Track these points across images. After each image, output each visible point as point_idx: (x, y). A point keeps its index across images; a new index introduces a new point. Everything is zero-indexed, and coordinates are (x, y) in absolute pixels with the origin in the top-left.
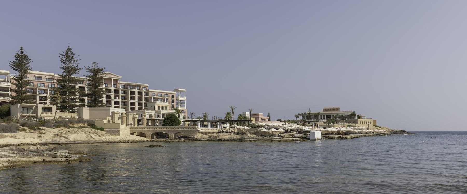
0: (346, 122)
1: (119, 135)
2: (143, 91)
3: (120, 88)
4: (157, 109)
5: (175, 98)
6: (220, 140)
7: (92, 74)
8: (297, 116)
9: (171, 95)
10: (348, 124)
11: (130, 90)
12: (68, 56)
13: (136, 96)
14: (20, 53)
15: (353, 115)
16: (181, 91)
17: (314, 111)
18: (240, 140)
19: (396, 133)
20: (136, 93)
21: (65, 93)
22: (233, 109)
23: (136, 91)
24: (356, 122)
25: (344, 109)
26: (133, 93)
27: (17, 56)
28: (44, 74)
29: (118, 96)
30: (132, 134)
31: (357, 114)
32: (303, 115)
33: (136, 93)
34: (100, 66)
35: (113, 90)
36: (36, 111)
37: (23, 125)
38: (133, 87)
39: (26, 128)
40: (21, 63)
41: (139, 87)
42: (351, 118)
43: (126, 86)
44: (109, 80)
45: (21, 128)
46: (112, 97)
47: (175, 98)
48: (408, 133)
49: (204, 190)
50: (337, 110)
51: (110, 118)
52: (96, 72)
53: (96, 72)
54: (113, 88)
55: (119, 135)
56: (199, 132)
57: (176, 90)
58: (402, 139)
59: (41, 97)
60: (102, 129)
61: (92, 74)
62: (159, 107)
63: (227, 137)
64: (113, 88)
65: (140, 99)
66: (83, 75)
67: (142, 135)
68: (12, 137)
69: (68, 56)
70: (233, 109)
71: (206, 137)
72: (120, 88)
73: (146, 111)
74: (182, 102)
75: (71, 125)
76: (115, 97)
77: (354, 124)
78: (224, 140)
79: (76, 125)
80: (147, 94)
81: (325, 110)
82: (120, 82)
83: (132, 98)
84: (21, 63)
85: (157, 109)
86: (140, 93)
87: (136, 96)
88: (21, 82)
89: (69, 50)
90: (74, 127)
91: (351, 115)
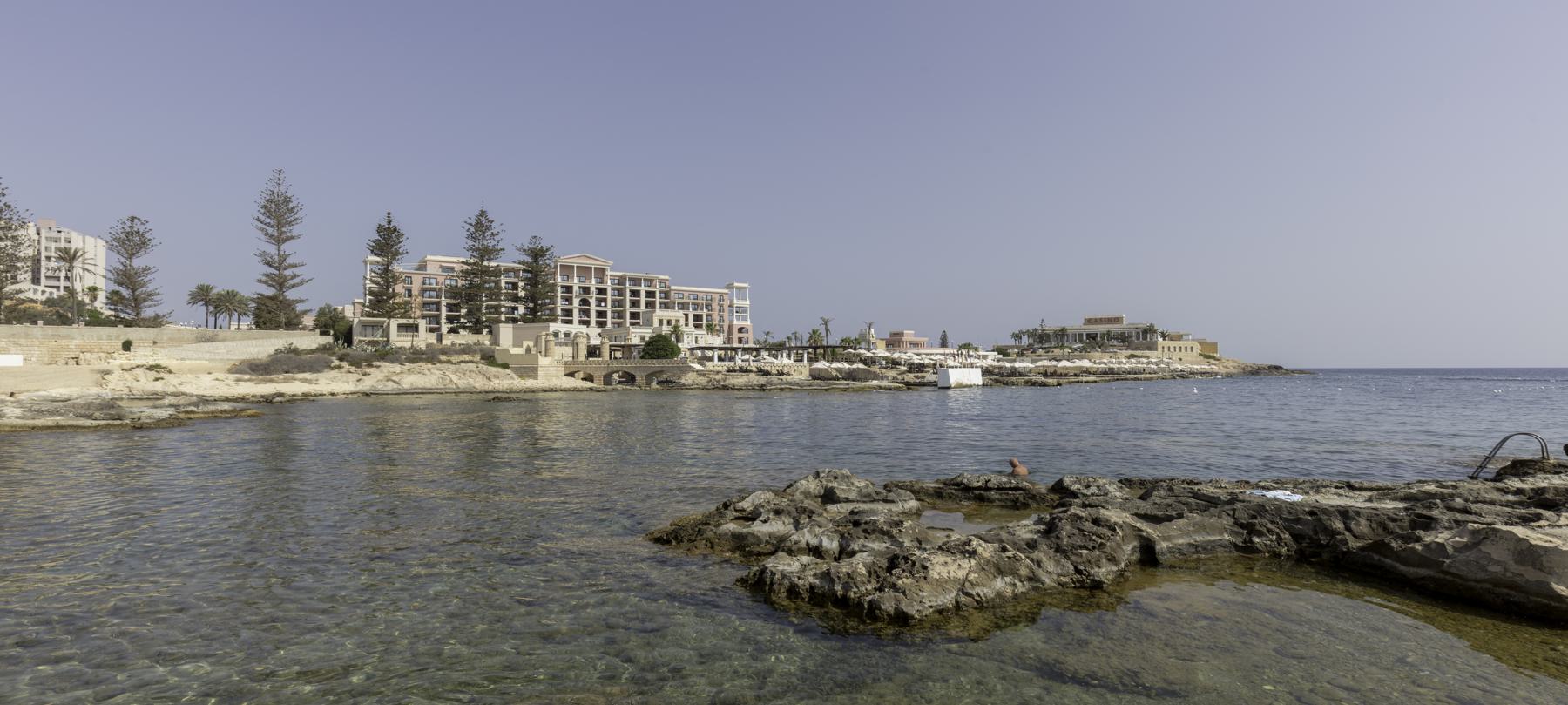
0: (1128, 348)
1: (536, 378)
2: (657, 289)
3: (608, 285)
4: (656, 324)
5: (727, 303)
6: (725, 387)
7: (529, 259)
8: (1017, 337)
9: (717, 297)
10: (1130, 352)
11: (629, 287)
12: (481, 226)
13: (643, 299)
14: (385, 223)
15: (1149, 331)
16: (739, 289)
17: (1052, 325)
18: (762, 388)
19: (1257, 371)
20: (643, 294)
21: (472, 301)
22: (826, 323)
23: (643, 290)
24: (1152, 347)
25: (1132, 319)
26: (635, 293)
27: (380, 229)
28: (436, 259)
29: (605, 300)
30: (571, 375)
31: (1159, 328)
32: (1031, 334)
33: (643, 294)
34: (545, 244)
35: (593, 289)
36: (386, 334)
37: (341, 359)
38: (636, 281)
39: (344, 364)
40: (387, 242)
41: (650, 281)
42: (1144, 338)
43: (622, 280)
44: (567, 269)
45: (337, 363)
46: (593, 302)
47: (727, 303)
48: (1288, 372)
49: (1353, 448)
50: (1117, 320)
51: (531, 344)
52: (537, 254)
53: (537, 254)
54: (593, 284)
55: (536, 378)
56: (693, 370)
57: (729, 287)
58: (1274, 385)
59: (448, 305)
60: (505, 366)
61: (529, 259)
62: (661, 322)
63: (740, 380)
64: (593, 284)
66: (510, 259)
67: (589, 378)
68: (305, 381)
69: (481, 226)
70: (826, 323)
71: (703, 381)
72: (608, 285)
73: (632, 330)
74: (740, 310)
75: (443, 357)
76: (600, 301)
77: (1147, 353)
78: (733, 388)
79: (455, 358)
80: (666, 295)
81: (1089, 321)
82: (609, 273)
83: (635, 304)
84: (387, 242)
85: (656, 324)
86: (650, 294)
87: (643, 299)
88: (387, 277)
89: (483, 213)
90: (448, 362)
91: (1145, 332)
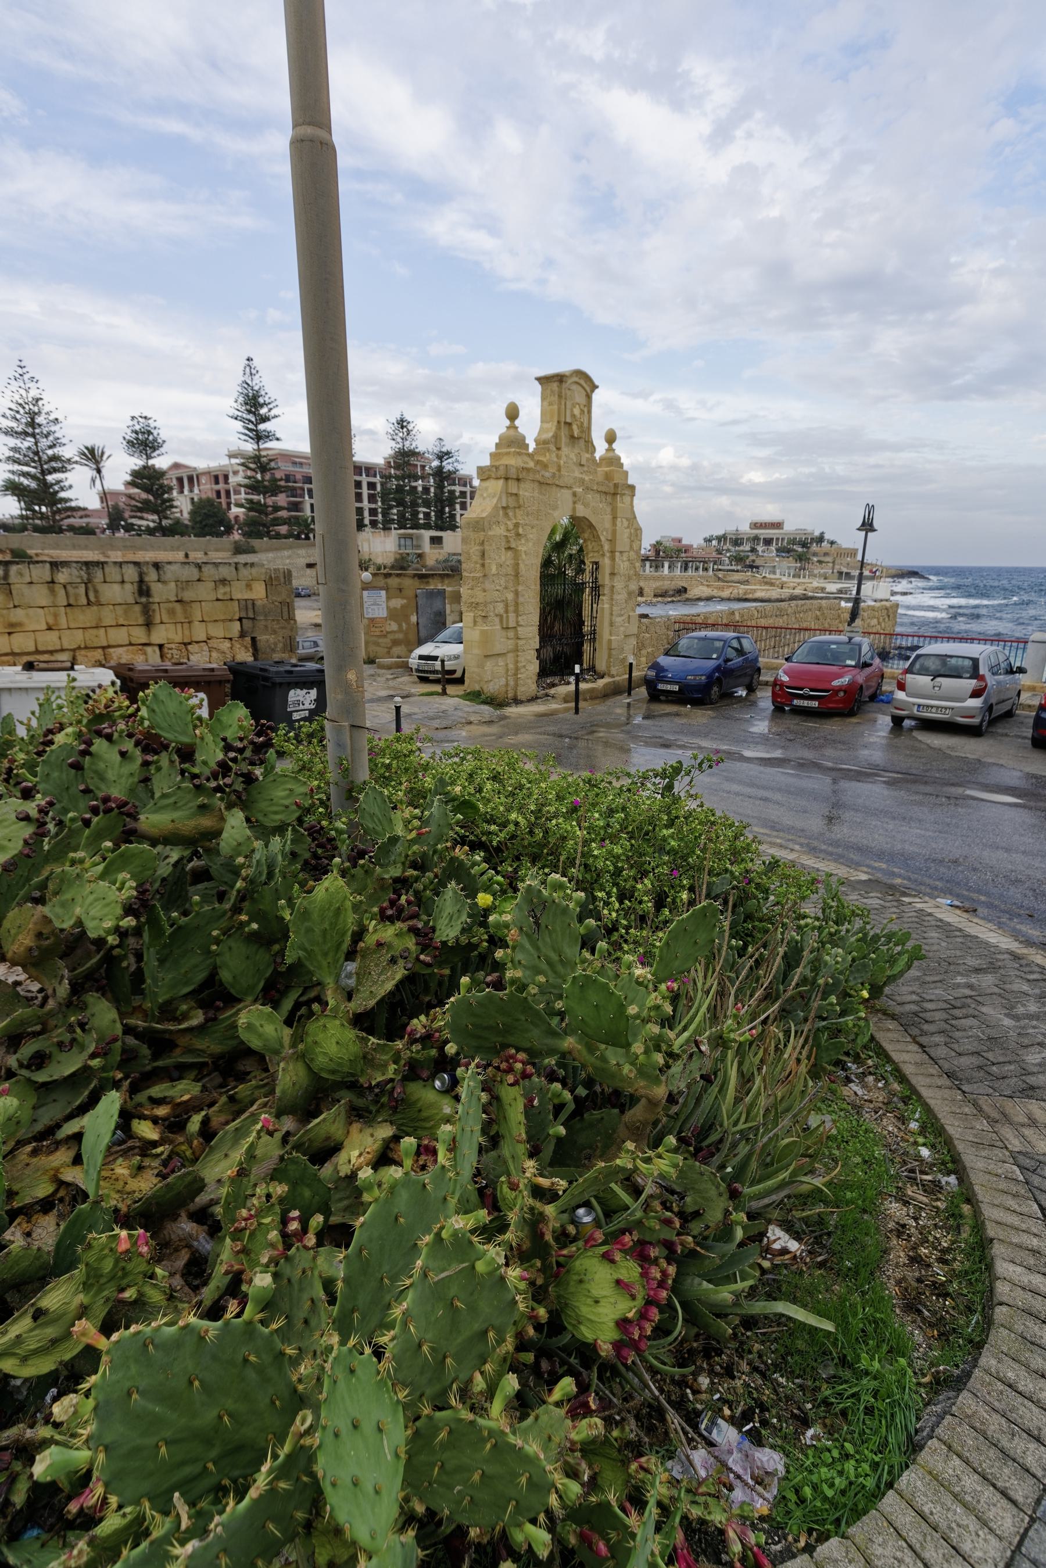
13: (365, 491)
65: (372, 498)
87: (365, 491)
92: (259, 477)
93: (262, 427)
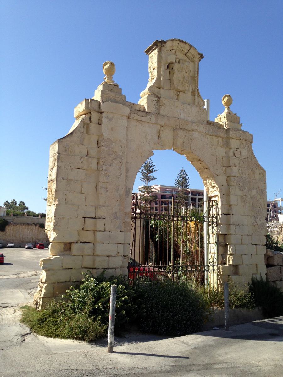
33: (197, 200)
92: (146, 195)
93: (149, 175)
